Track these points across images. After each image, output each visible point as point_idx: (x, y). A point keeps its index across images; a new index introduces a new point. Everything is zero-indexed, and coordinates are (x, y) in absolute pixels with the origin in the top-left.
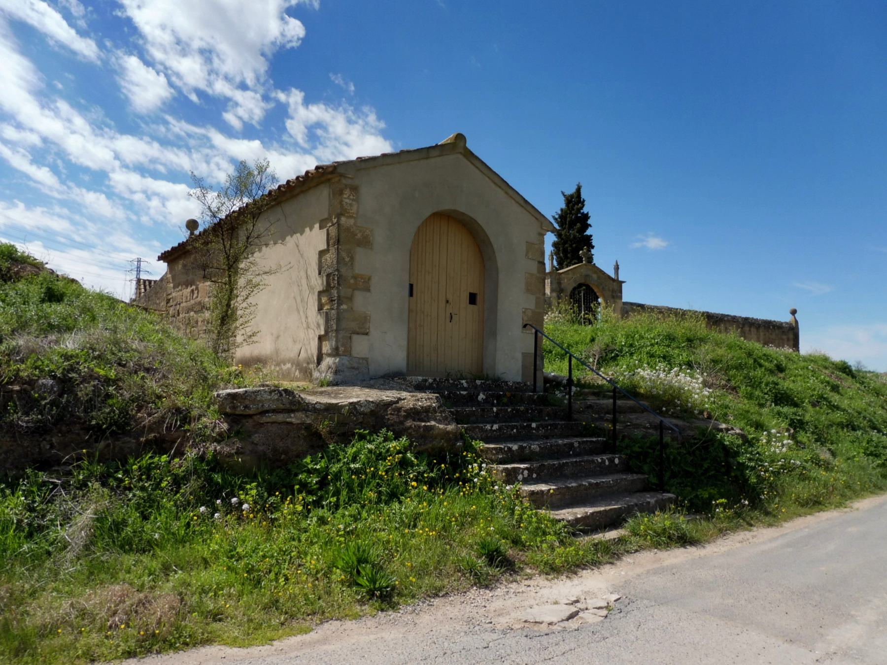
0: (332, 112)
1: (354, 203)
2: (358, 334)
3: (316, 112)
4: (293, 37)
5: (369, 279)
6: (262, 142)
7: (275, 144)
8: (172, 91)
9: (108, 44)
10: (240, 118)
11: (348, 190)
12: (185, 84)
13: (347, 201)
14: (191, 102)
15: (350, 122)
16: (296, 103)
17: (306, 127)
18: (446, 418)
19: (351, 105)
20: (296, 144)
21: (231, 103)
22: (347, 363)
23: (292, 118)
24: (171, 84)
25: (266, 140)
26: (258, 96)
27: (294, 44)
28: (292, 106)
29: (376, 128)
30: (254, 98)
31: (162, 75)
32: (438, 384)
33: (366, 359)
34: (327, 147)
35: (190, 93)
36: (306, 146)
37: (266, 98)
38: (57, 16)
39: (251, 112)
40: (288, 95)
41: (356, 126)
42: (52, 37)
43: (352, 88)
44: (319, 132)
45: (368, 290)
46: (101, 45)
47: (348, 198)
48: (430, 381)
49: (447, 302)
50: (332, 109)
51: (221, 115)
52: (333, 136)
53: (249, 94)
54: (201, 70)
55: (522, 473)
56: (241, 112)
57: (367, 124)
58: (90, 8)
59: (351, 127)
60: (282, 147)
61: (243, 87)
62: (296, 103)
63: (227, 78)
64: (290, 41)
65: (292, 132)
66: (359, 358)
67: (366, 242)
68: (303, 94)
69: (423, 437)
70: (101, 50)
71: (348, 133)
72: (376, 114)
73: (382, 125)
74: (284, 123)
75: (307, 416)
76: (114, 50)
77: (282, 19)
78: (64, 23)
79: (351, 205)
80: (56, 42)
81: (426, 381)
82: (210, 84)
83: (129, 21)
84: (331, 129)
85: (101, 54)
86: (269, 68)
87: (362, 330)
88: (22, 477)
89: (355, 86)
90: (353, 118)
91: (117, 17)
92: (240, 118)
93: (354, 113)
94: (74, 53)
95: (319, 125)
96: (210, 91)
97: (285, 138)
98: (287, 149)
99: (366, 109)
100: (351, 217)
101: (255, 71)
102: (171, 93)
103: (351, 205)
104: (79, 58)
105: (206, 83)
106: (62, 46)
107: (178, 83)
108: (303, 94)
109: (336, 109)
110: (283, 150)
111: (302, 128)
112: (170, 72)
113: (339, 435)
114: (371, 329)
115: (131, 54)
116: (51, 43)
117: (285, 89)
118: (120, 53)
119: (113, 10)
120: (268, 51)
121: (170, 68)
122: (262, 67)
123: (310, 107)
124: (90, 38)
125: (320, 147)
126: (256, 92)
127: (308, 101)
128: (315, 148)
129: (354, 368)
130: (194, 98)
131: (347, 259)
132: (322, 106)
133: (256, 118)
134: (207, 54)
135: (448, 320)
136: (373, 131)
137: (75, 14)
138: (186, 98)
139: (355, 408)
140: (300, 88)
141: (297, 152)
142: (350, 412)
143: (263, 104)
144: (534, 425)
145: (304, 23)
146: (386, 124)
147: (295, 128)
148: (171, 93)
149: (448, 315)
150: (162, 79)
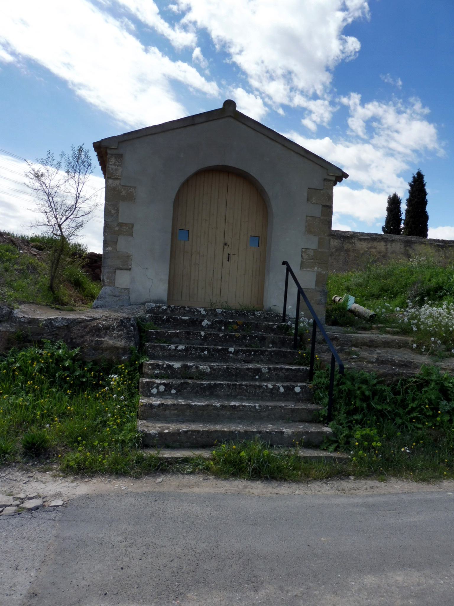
0: (384, 107)
1: (119, 168)
2: (121, 269)
3: (372, 108)
4: (351, 52)
5: (133, 225)
6: (331, 138)
7: (341, 139)
8: (267, 109)
9: (224, 82)
10: (315, 122)
11: (114, 158)
12: (274, 102)
13: (113, 166)
14: (279, 114)
15: (399, 112)
16: (355, 104)
17: (364, 122)
18: (120, 336)
19: (399, 98)
20: (358, 137)
21: (307, 112)
22: (110, 292)
23: (352, 116)
24: (265, 104)
25: (334, 136)
26: (326, 103)
27: (352, 58)
28: (352, 108)
29: (421, 114)
30: (323, 105)
31: (258, 97)
32: (172, 310)
33: (128, 289)
34: (381, 136)
35: (278, 108)
36: (365, 137)
37: (332, 103)
38: (193, 71)
39: (322, 117)
40: (349, 98)
41: (404, 115)
42: (191, 86)
43: (400, 83)
44: (375, 124)
45: (131, 235)
46: (220, 85)
47: (114, 164)
48: (164, 307)
49: (225, 244)
50: (384, 104)
51: (301, 121)
52: (386, 126)
53: (319, 102)
54: (285, 89)
55: (157, 388)
56: (314, 117)
57: (414, 112)
58: (211, 60)
59: (400, 116)
60: (346, 140)
61: (315, 97)
62: (355, 104)
63: (302, 93)
64: (350, 56)
65: (353, 127)
66: (121, 288)
67: (130, 198)
68: (360, 96)
69: (95, 349)
70: (220, 89)
71: (398, 122)
72: (421, 102)
73: (427, 111)
74: (347, 121)
75: (11, 327)
76: (227, 86)
77: (341, 39)
78: (198, 74)
79: (116, 170)
80: (194, 88)
81: (159, 307)
82: (291, 99)
83: (234, 64)
84: (384, 121)
85: (221, 91)
86: (333, 80)
87: (126, 267)
88: (34, 382)
89: (402, 80)
90: (402, 109)
91: (227, 64)
92: (315, 122)
93: (402, 104)
94: (205, 93)
95: (375, 119)
96: (292, 105)
97: (348, 133)
98: (350, 141)
99: (412, 100)
100: (117, 179)
101: (323, 84)
102: (266, 111)
103: (116, 170)
104: (208, 96)
105: (288, 99)
106: (198, 90)
107: (270, 102)
108: (360, 96)
109: (387, 104)
110: (347, 143)
111: (361, 123)
112: (263, 95)
113: (99, 349)
114: (132, 266)
115: (237, 87)
116: (191, 90)
117: (346, 94)
118: (231, 88)
119: (224, 59)
120: (332, 67)
121: (264, 93)
122: (326, 78)
123: (366, 106)
124: (213, 81)
125: (375, 136)
126: (324, 99)
127: (363, 102)
128: (372, 137)
129: (115, 296)
130: (281, 111)
131: (113, 212)
132: (376, 103)
133: (326, 120)
134: (288, 76)
135: (226, 259)
136: (418, 117)
137: (203, 67)
138: (276, 112)
139: (51, 322)
140: (358, 91)
141: (358, 143)
142: (45, 326)
143: (330, 109)
144: (231, 349)
145: (360, 39)
146: (430, 109)
147: (356, 124)
148: (266, 111)
149: (226, 256)
150: (259, 101)
